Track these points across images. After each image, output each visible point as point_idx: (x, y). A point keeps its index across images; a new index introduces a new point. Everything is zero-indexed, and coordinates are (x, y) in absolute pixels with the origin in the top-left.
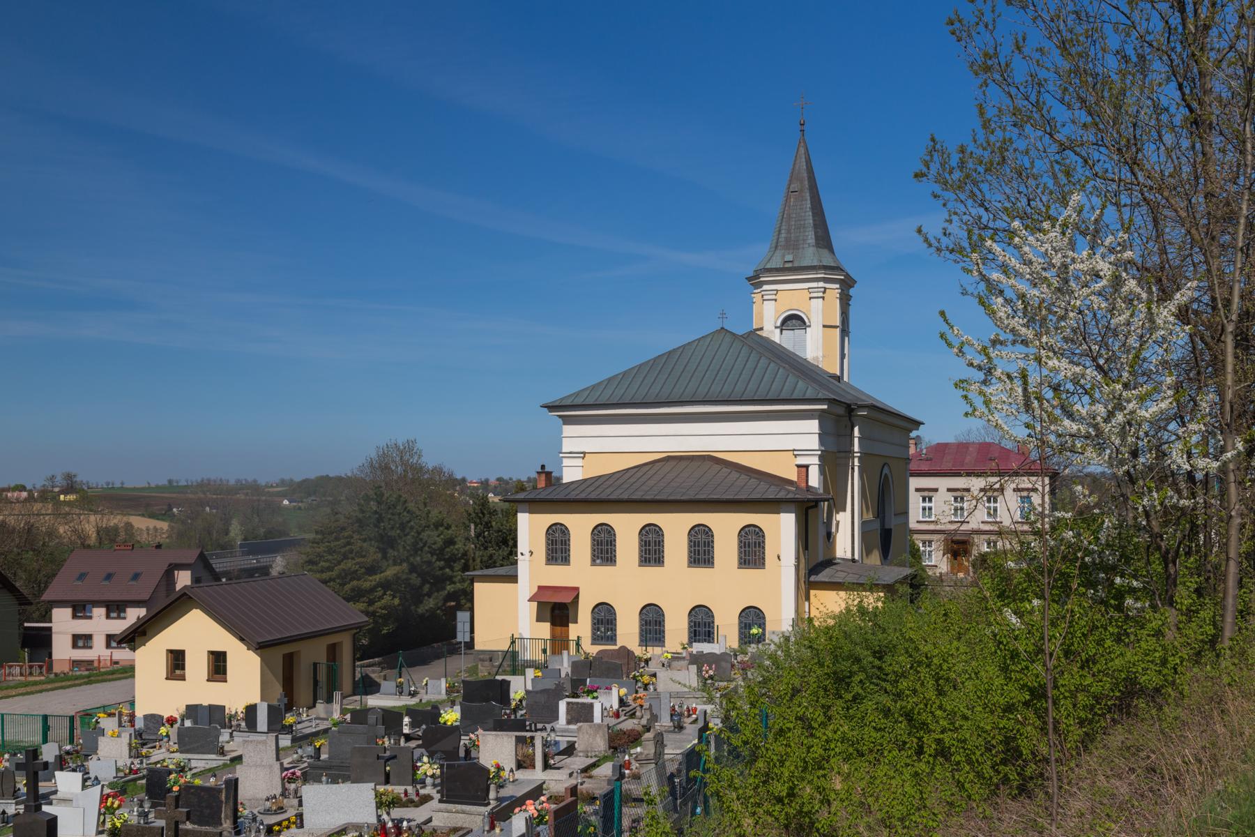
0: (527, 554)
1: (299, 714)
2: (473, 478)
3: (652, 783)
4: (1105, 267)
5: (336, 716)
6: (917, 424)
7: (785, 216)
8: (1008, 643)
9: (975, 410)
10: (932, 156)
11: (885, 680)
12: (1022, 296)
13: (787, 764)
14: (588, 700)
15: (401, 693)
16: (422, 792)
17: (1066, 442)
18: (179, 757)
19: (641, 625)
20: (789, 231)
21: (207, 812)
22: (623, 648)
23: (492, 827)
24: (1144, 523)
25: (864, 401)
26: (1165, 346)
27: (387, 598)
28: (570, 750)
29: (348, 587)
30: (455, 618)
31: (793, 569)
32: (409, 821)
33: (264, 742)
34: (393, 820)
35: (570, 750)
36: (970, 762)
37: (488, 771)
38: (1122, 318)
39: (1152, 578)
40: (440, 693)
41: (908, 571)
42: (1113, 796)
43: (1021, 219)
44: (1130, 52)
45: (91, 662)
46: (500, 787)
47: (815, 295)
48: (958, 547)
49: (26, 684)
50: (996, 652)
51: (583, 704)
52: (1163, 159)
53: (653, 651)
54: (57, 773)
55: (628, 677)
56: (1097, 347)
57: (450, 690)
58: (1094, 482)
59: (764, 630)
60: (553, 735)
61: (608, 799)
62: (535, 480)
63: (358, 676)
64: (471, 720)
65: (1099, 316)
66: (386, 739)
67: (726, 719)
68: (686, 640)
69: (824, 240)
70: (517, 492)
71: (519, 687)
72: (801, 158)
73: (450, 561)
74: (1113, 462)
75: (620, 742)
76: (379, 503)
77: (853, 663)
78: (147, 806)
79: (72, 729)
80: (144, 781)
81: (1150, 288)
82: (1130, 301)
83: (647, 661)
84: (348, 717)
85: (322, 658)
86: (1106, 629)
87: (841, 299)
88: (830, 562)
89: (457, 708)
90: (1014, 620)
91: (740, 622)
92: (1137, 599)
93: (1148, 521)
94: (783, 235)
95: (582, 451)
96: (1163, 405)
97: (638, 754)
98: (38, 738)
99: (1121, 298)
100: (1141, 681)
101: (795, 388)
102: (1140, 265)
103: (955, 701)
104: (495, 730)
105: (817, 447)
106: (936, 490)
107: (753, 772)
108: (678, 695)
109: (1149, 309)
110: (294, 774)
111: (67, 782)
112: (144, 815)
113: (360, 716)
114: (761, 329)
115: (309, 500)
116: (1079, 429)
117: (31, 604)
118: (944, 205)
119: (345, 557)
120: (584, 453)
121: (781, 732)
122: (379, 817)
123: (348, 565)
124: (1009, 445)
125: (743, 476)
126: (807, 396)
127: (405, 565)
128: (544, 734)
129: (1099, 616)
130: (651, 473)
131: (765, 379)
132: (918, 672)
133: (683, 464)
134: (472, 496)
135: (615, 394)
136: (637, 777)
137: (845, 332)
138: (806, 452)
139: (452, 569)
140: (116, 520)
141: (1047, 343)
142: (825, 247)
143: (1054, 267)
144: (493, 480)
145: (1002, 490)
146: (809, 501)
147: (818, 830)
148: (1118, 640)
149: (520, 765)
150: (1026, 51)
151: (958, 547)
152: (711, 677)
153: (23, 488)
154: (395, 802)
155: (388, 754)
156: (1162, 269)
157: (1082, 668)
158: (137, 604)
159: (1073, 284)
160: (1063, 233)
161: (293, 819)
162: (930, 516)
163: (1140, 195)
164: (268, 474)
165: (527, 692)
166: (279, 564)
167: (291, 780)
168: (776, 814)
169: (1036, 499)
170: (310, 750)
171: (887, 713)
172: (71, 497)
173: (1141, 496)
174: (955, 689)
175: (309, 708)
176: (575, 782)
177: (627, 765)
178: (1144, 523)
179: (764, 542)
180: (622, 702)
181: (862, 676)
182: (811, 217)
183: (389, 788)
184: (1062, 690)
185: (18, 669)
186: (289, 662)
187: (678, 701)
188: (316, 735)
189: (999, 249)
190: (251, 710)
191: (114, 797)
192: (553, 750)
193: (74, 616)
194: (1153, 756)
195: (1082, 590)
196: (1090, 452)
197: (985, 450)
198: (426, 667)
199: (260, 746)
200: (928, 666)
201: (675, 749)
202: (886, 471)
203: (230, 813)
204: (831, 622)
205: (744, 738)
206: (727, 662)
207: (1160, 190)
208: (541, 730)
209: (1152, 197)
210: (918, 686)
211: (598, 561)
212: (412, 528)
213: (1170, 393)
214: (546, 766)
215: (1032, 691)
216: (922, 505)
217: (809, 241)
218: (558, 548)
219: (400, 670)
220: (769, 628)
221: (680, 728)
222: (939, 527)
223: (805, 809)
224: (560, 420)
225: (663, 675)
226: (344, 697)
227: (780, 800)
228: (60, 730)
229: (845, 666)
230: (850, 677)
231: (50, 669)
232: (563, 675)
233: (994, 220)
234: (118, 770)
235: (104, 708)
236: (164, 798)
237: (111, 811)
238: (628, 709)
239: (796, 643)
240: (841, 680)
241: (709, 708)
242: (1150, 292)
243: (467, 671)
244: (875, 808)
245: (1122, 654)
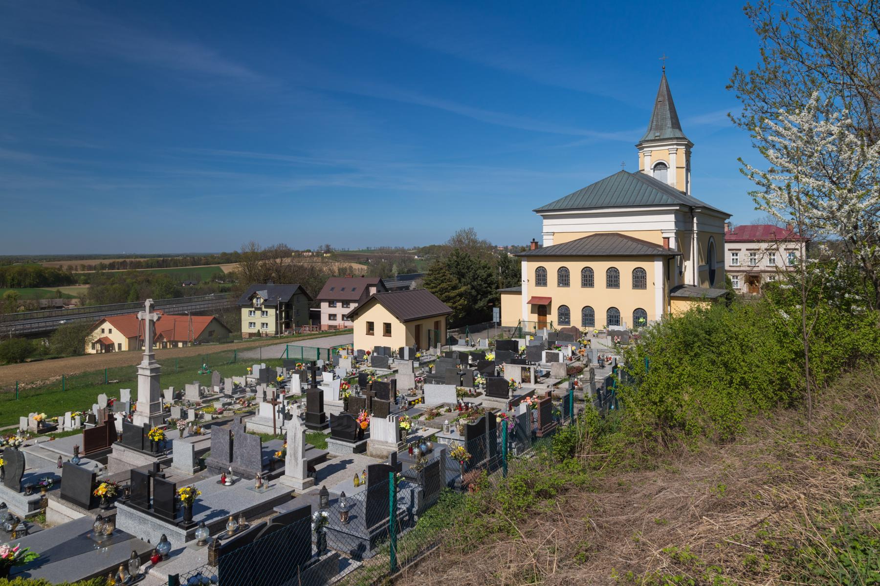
0: (526, 281)
1: (422, 353)
2: (501, 247)
3: (588, 392)
4: (835, 129)
5: (439, 354)
6: (729, 216)
8: (782, 328)
9: (761, 206)
10: (736, 77)
11: (712, 346)
12: (786, 147)
13: (659, 385)
14: (556, 351)
15: (467, 345)
16: (477, 391)
17: (815, 222)
18: (371, 369)
19: (583, 316)
20: (657, 121)
21: (383, 393)
22: (574, 327)
23: (510, 409)
24: (862, 265)
26: (872, 169)
27: (462, 301)
28: (548, 375)
29: (444, 295)
30: (492, 311)
31: (662, 289)
32: (472, 404)
33: (407, 364)
34: (464, 403)
35: (548, 375)
36: (760, 389)
37: (508, 383)
38: (846, 155)
39: (867, 294)
40: (485, 346)
41: (724, 291)
42: (845, 410)
43: (786, 106)
44: (849, 14)
45: (335, 327)
46: (514, 390)
47: (672, 152)
48: (752, 279)
49: (311, 335)
50: (775, 333)
51: (554, 353)
52: (870, 70)
53: (588, 329)
54: (323, 373)
55: (576, 341)
56: (832, 172)
57: (490, 344)
58: (832, 245)
59: (646, 320)
60: (539, 367)
61: (567, 399)
62: (530, 246)
63: (448, 337)
64: (500, 359)
65: (833, 156)
66: (461, 366)
67: (627, 363)
68: (605, 324)
69: (676, 125)
70: (521, 252)
71: (522, 344)
73: (490, 284)
74: (844, 231)
75: (572, 372)
76: (458, 257)
77: (694, 337)
78: (359, 389)
79: (329, 355)
80: (357, 379)
81: (862, 138)
82: (850, 146)
83: (586, 334)
84: (444, 355)
85: (432, 328)
86: (840, 321)
87: (686, 154)
88: (681, 286)
89: (494, 353)
90: (785, 316)
91: (634, 316)
92: (858, 306)
93: (865, 264)
96: (873, 201)
97: (581, 379)
98: (315, 358)
99: (845, 145)
100: (861, 350)
102: (857, 127)
103: (752, 357)
104: (511, 363)
106: (740, 250)
107: (641, 389)
108: (602, 351)
109: (863, 149)
110: (420, 379)
111: (327, 377)
112: (358, 393)
113: (449, 354)
114: (643, 170)
115: (426, 256)
116: (822, 214)
117: (313, 300)
118: (743, 102)
119: (442, 282)
120: (554, 233)
121: (656, 369)
122: (458, 401)
123: (444, 285)
124: (781, 225)
125: (634, 243)
126: (668, 203)
127: (469, 285)
128: (535, 367)
129: (835, 314)
130: (587, 242)
132: (731, 342)
133: (604, 237)
134: (500, 254)
136: (581, 389)
137: (688, 170)
138: (668, 231)
139: (491, 288)
140: (346, 265)
141: (801, 170)
142: (677, 128)
143: (805, 131)
144: (510, 247)
145: (777, 249)
146: (670, 255)
147: (676, 420)
148: (847, 327)
149: (523, 381)
150: (788, 20)
151: (752, 279)
152: (619, 342)
153: (309, 251)
154: (465, 395)
155: (462, 372)
156: (870, 129)
157: (826, 342)
158: (354, 301)
159: (816, 138)
160: (809, 112)
161: (420, 399)
162: (737, 263)
163: (856, 91)
164: (408, 245)
165: (527, 347)
166: (413, 284)
167: (419, 382)
168: (653, 410)
169: (798, 254)
170: (427, 369)
171: (713, 363)
172: (328, 255)
173: (860, 250)
174: (752, 351)
175: (427, 350)
176: (550, 390)
177: (576, 383)
178: (862, 265)
179: (646, 276)
180: (573, 353)
181: (699, 344)
183: (463, 388)
184: (814, 353)
185: (308, 328)
186: (418, 328)
187: (602, 354)
188: (430, 362)
189: (772, 124)
190: (402, 350)
191: (346, 384)
192: (539, 374)
193: (330, 306)
194: (869, 390)
195: (825, 300)
196: (829, 227)
197: (767, 228)
198: (478, 333)
199: (406, 366)
200: (736, 339)
201: (600, 376)
202: (712, 240)
203: (393, 395)
204: (683, 316)
205: (636, 372)
206: (627, 335)
207: (868, 87)
208: (533, 365)
209: (863, 91)
210: (731, 349)
211: (561, 285)
212: (472, 268)
213: (876, 194)
214: (536, 382)
215: (796, 353)
216: (732, 257)
218: (541, 278)
220: (649, 319)
221: (603, 367)
222: (742, 269)
223: (669, 409)
225: (593, 340)
226: (442, 346)
227: (655, 403)
228: (324, 355)
229: (690, 338)
230: (693, 344)
231: (320, 328)
232: (544, 339)
233: (771, 108)
234: (347, 373)
235: (341, 346)
236: (366, 386)
237: (344, 390)
238: (576, 357)
239: (663, 326)
240: (688, 346)
241: (618, 357)
242: (863, 140)
243: (499, 336)
244: (707, 410)
245: (849, 335)
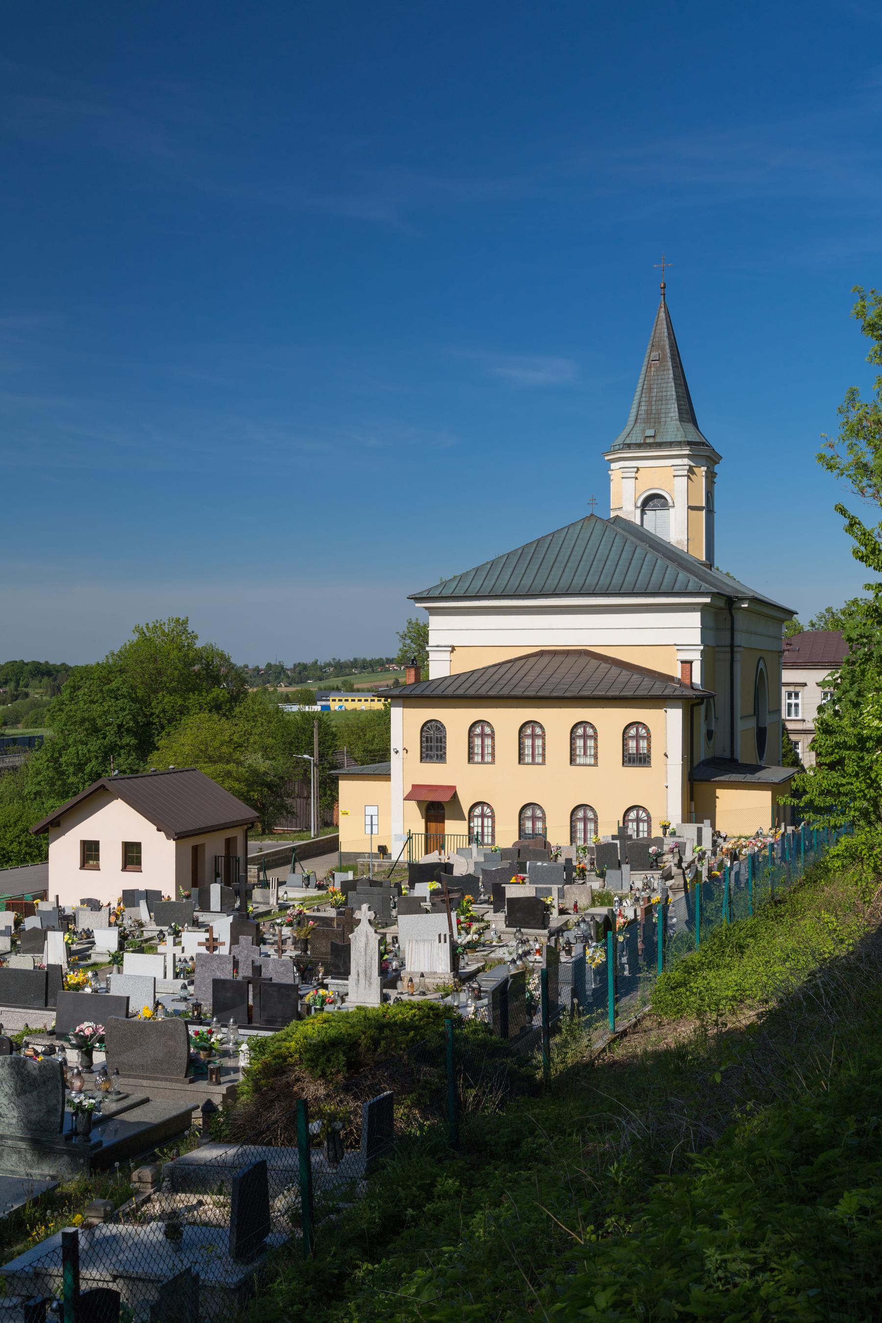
6: (792, 613)
7: (645, 387)
25: (744, 593)
69: (688, 414)
72: (662, 324)
87: (707, 477)
94: (643, 408)
95: (450, 644)
101: (676, 580)
105: (699, 643)
106: (805, 685)
120: (453, 648)
131: (643, 571)
133: (558, 659)
135: (484, 586)
162: (797, 714)
182: (674, 388)
186: (196, 851)
202: (761, 665)
217: (672, 415)
219: (294, 865)
224: (427, 611)
